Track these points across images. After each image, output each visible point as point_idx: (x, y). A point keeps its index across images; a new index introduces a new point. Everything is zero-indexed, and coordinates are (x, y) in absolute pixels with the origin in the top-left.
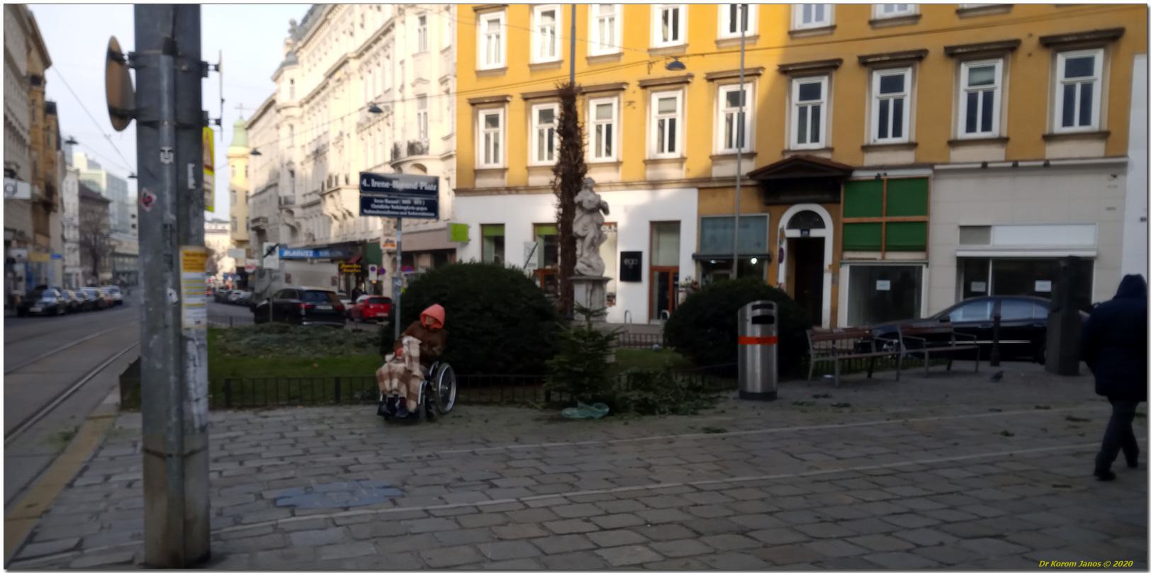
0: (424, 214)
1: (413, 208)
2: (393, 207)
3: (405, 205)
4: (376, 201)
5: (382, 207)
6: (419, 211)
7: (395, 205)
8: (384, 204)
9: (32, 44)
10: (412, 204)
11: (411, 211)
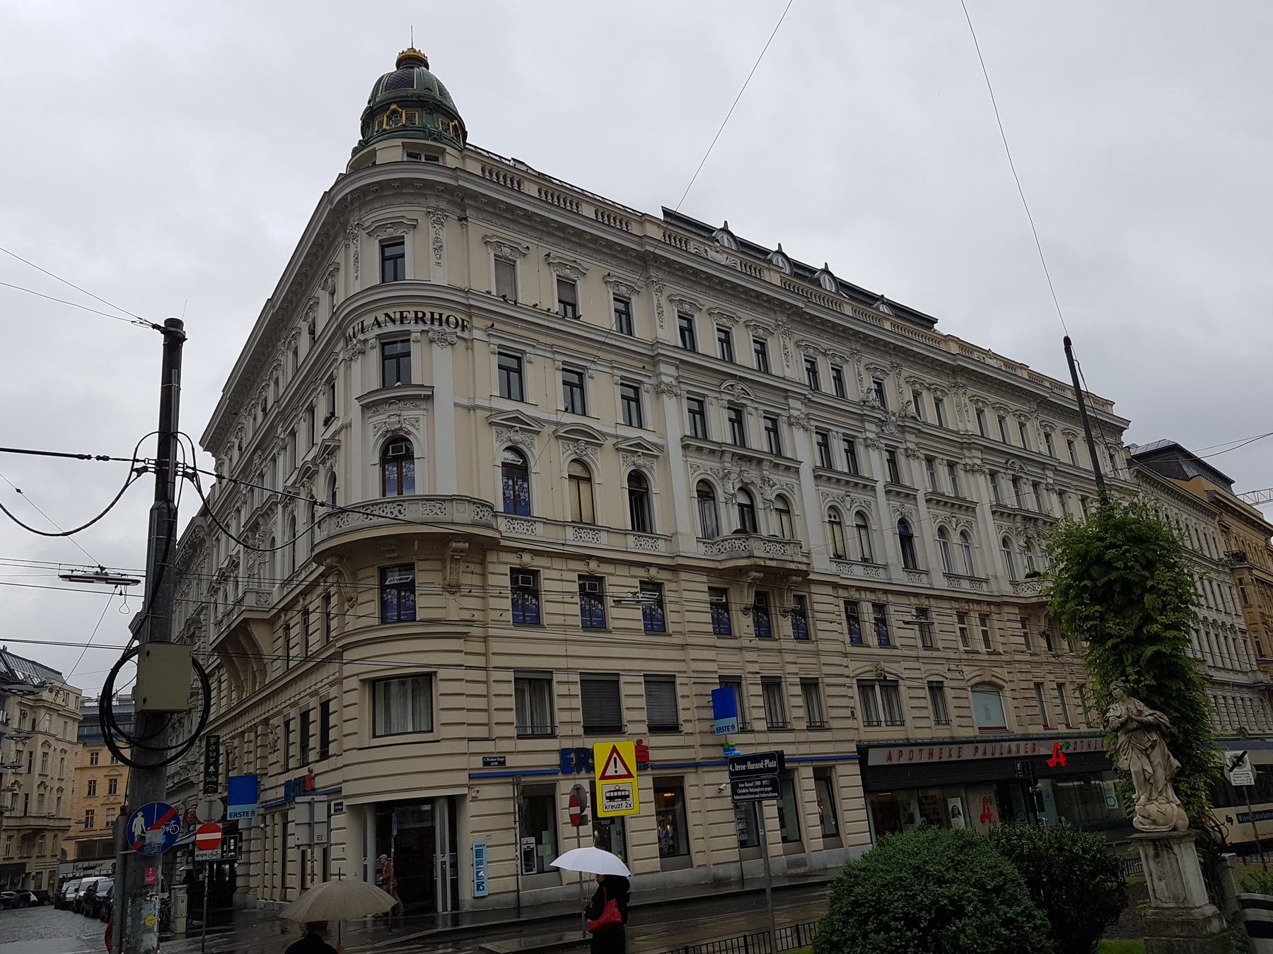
0: (770, 795)
1: (763, 789)
2: (752, 790)
3: (757, 787)
4: (740, 785)
5: (744, 791)
6: (767, 792)
7: (751, 787)
8: (745, 787)
9: (1228, 519)
10: (762, 786)
11: (762, 792)
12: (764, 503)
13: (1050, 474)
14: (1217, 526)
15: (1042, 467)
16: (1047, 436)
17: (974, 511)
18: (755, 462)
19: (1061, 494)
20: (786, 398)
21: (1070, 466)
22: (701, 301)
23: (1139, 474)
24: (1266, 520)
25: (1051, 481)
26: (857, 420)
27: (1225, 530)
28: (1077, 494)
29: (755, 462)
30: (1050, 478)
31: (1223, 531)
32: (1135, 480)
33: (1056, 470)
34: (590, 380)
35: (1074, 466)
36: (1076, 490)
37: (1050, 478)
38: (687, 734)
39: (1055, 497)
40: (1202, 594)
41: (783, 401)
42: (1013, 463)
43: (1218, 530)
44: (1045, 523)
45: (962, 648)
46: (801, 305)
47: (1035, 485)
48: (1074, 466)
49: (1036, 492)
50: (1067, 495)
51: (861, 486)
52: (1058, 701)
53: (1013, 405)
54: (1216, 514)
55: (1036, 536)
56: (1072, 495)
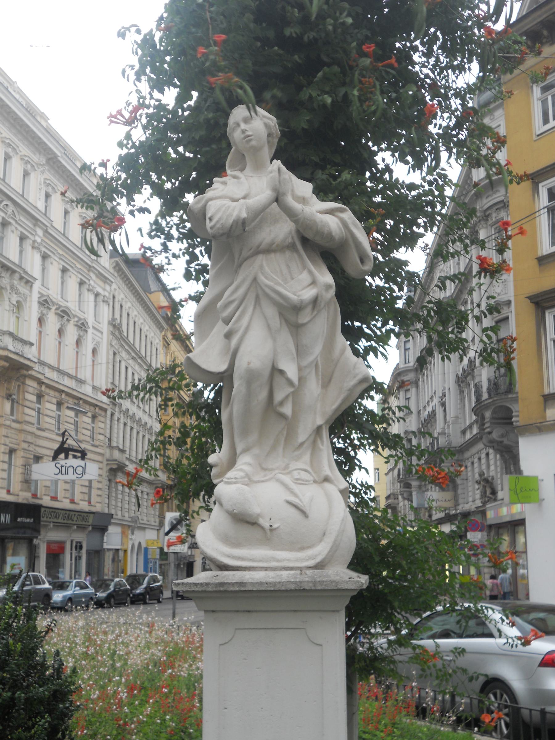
12: (10, 306)
13: (40, 232)
14: (161, 339)
15: (34, 222)
16: (48, 196)
17: (31, 286)
18: (10, 272)
19: (45, 257)
20: (35, 225)
21: (78, 247)
22: (21, 149)
23: (117, 266)
24: (12, 185)
25: (39, 240)
26: (86, 268)
27: (167, 345)
28: (59, 264)
29: (10, 272)
30: (39, 236)
31: (164, 345)
32: (112, 271)
33: (46, 232)
34: (12, 234)
35: (64, 235)
36: (61, 259)
37: (39, 236)
38: (48, 495)
39: (37, 258)
40: (33, 339)
41: (86, 271)
42: (7, 205)
43: (161, 343)
44: (21, 278)
45: (36, 425)
46: (59, 154)
47: (22, 238)
48: (64, 235)
49: (21, 245)
50: (69, 274)
51: (24, 280)
52: (6, 466)
53: (24, 150)
54: (163, 328)
55: (8, 288)
56: (54, 262)
